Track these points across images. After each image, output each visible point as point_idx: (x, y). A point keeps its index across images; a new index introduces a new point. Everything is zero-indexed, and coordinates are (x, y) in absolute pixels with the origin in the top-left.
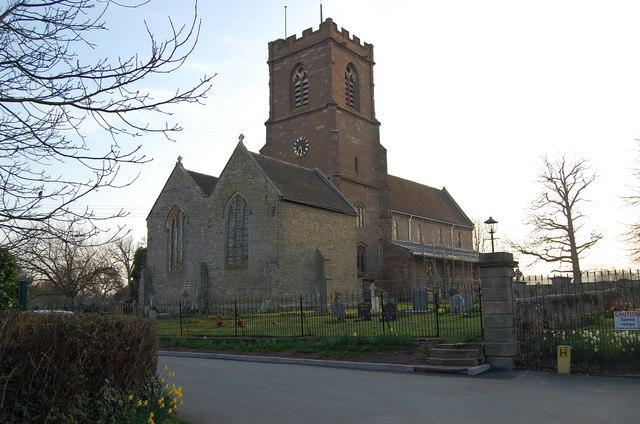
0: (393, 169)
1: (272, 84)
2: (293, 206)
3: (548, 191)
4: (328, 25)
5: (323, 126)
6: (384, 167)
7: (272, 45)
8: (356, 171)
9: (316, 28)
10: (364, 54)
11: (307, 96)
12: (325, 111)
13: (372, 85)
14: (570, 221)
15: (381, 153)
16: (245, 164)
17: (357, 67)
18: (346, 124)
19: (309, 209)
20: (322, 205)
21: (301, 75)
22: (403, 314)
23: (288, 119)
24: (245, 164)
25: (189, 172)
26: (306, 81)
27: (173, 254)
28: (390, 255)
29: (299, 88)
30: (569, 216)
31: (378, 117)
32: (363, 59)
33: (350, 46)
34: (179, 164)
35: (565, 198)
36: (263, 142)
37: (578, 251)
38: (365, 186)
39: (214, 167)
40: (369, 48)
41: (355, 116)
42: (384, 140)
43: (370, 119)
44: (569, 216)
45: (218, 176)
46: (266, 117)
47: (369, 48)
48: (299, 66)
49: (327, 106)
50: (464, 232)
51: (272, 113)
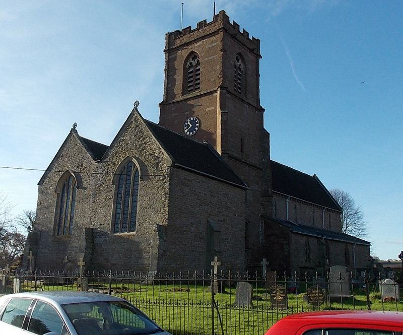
6: (266, 150)
9: (210, 19)
13: (258, 75)
15: (264, 137)
17: (245, 57)
27: (60, 219)
31: (262, 104)
32: (252, 51)
33: (240, 38)
34: (74, 130)
38: (250, 165)
39: (104, 136)
41: (243, 101)
42: (268, 125)
43: (255, 105)
45: (109, 146)
47: (258, 41)
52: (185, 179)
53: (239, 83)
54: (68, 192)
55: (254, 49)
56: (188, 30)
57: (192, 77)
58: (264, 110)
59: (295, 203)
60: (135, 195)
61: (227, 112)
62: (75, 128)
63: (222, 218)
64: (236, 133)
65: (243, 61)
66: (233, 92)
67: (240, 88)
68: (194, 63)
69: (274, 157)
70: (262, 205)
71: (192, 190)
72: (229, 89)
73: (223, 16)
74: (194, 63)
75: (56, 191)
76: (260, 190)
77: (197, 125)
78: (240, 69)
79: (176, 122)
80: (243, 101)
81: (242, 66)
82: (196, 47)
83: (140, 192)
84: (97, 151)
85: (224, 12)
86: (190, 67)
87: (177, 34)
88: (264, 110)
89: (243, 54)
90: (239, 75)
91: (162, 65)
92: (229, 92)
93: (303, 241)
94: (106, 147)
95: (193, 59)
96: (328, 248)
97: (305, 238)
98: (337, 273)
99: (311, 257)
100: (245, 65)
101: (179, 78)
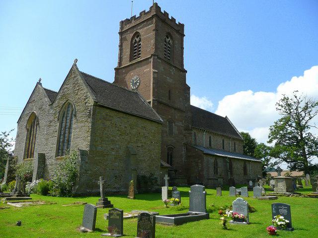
13: (183, 48)
18: (164, 69)
19: (121, 115)
27: (29, 149)
29: (136, 51)
31: (185, 67)
32: (178, 31)
33: (169, 22)
34: (39, 83)
38: (175, 109)
40: (182, 26)
41: (171, 65)
43: (180, 68)
46: (116, 65)
47: (182, 26)
49: (151, 57)
52: (107, 115)
54: (34, 128)
55: (179, 30)
56: (134, 18)
60: (70, 128)
63: (140, 145)
65: (172, 38)
66: (164, 59)
68: (137, 40)
69: (192, 104)
72: (161, 57)
73: (156, 7)
74: (137, 40)
75: (26, 127)
76: (183, 126)
80: (171, 65)
81: (171, 42)
83: (74, 126)
84: (51, 94)
85: (156, 4)
86: (135, 43)
87: (128, 21)
89: (172, 33)
90: (169, 47)
91: (118, 42)
92: (160, 59)
93: (212, 160)
97: (214, 158)
98: (171, 188)
99: (218, 170)
101: (127, 51)
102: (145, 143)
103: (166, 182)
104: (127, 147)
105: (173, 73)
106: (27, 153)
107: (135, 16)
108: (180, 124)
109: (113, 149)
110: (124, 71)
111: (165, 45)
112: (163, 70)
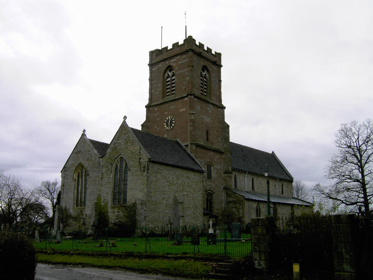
0: (235, 137)
1: (151, 80)
2: (158, 165)
3: (348, 155)
4: (190, 40)
5: (185, 109)
6: (228, 138)
7: (152, 53)
8: (207, 140)
9: (181, 42)
10: (215, 59)
11: (174, 88)
12: (186, 99)
13: (220, 81)
14: (363, 176)
16: (127, 135)
17: (210, 69)
18: (201, 107)
19: (169, 168)
20: (168, 162)
21: (170, 74)
22: (55, 210)
23: (161, 104)
24: (127, 135)
25: (90, 140)
26: (174, 78)
28: (231, 199)
29: (169, 83)
30: (362, 173)
31: (224, 103)
34: (83, 135)
35: (360, 161)
36: (143, 119)
37: (368, 198)
40: (219, 55)
41: (208, 102)
43: (218, 104)
44: (362, 173)
45: (109, 143)
46: (147, 102)
47: (219, 55)
48: (170, 68)
50: (285, 184)
51: (151, 99)
52: (158, 169)
53: (205, 88)
54: (82, 178)
57: (169, 85)
58: (225, 108)
59: (253, 176)
61: (194, 113)
62: (84, 133)
63: (185, 194)
64: (202, 127)
65: (208, 71)
67: (205, 92)
70: (224, 179)
71: (163, 176)
72: (197, 94)
77: (173, 122)
78: (206, 78)
79: (158, 119)
81: (207, 75)
82: (172, 62)
84: (100, 147)
86: (168, 77)
88: (225, 108)
90: (205, 82)
93: (255, 205)
94: (106, 145)
95: (170, 71)
96: (275, 211)
100: (210, 74)
102: (189, 192)
103: (211, 225)
104: (175, 196)
105: (210, 111)
106: (75, 202)
107: (167, 48)
108: (219, 167)
109: (164, 198)
110: (156, 109)
111: (201, 80)
112: (200, 109)
